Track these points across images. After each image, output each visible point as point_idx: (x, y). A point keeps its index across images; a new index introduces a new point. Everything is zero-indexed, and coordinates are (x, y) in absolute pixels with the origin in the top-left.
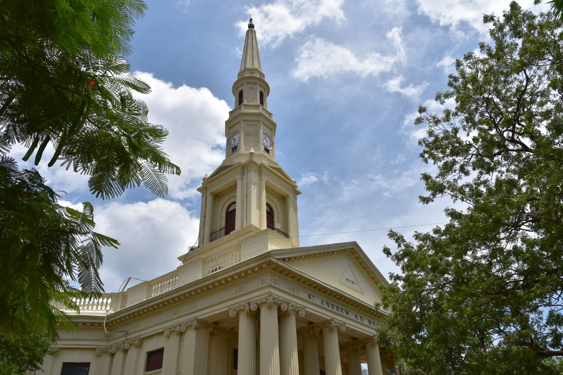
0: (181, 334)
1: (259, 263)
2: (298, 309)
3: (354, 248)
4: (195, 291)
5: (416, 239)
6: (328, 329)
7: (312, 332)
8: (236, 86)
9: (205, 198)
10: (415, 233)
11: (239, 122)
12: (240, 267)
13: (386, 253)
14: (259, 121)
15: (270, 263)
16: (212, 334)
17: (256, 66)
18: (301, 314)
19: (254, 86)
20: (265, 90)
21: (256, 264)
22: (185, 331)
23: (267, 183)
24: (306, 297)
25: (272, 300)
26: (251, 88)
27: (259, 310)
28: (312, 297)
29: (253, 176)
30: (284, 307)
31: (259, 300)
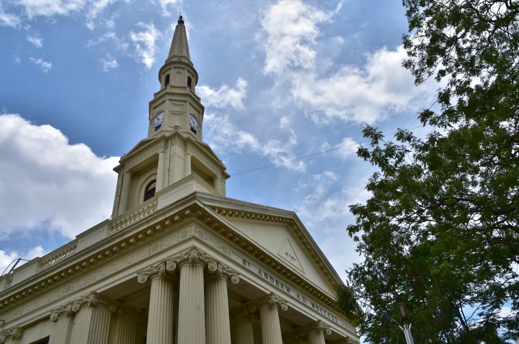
0: (73, 315)
1: (180, 209)
2: (230, 274)
3: (292, 219)
4: (95, 256)
5: (398, 139)
6: (266, 307)
7: (246, 312)
8: (162, 71)
9: (121, 177)
10: (397, 131)
11: (164, 101)
12: (155, 218)
13: (363, 156)
14: (185, 101)
15: (195, 208)
16: (114, 316)
17: (184, 54)
18: (235, 280)
19: (182, 71)
20: (193, 76)
21: (176, 211)
22: (78, 311)
23: (193, 158)
24: (241, 262)
25: (196, 255)
26: (179, 73)
27: (177, 272)
28: (247, 264)
29: (177, 149)
30: (213, 267)
31: (178, 258)
